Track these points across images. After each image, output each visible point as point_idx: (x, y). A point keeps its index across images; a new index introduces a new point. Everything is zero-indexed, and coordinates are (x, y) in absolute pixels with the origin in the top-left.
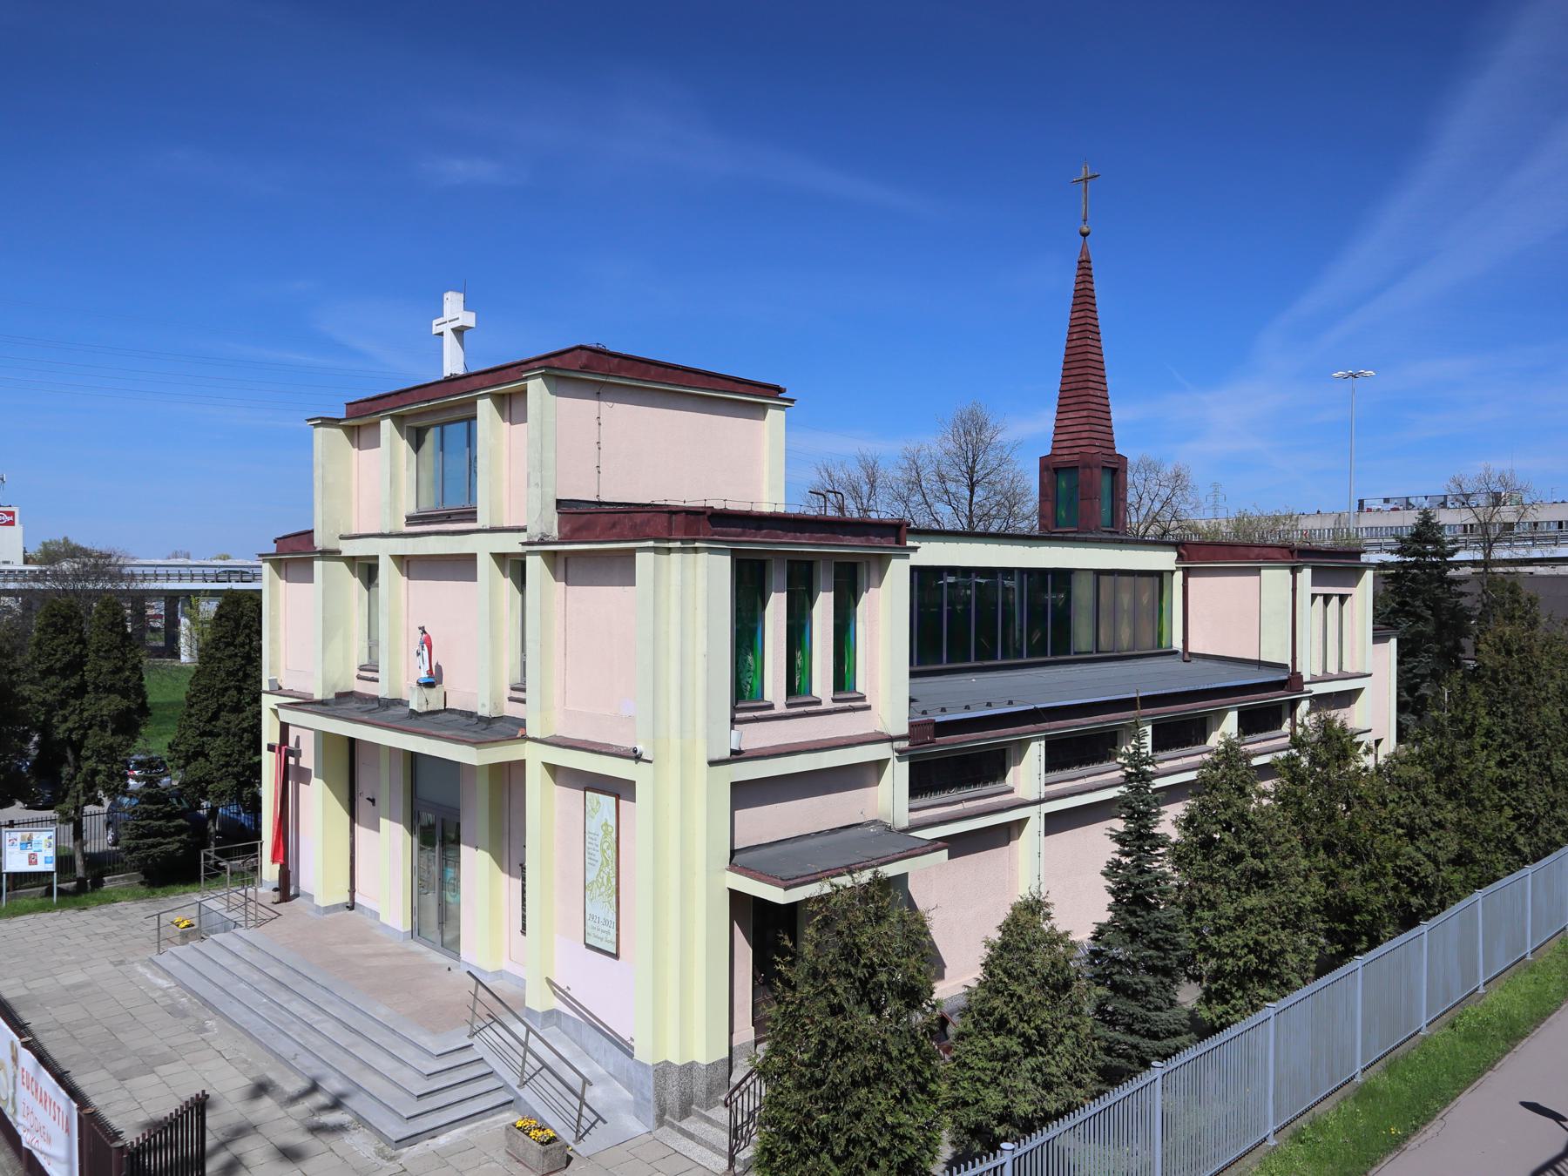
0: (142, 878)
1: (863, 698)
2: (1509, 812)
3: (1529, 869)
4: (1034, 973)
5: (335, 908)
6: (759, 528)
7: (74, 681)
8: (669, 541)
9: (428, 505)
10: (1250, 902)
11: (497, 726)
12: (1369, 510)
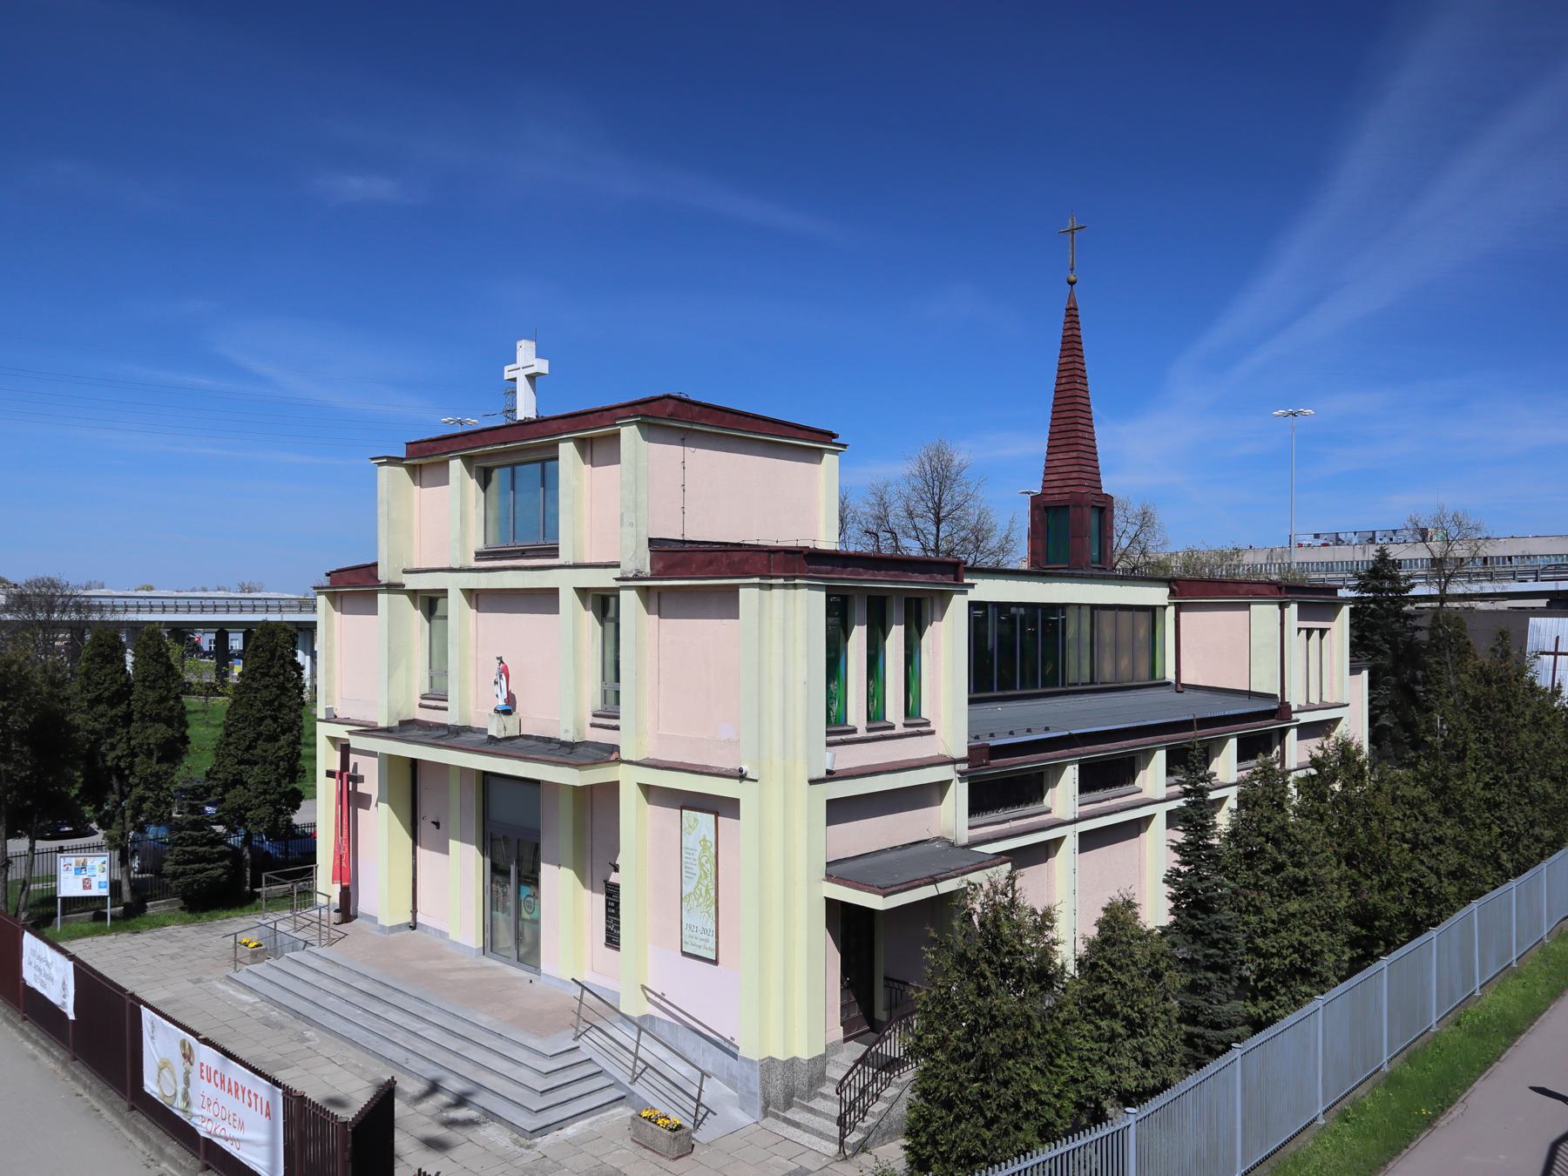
0: (182, 903)
1: (927, 724)
2: (1496, 830)
3: (1513, 883)
4: (1135, 963)
5: (399, 927)
6: (845, 566)
8: (772, 577)
9: (494, 543)
10: (1293, 906)
11: (581, 750)
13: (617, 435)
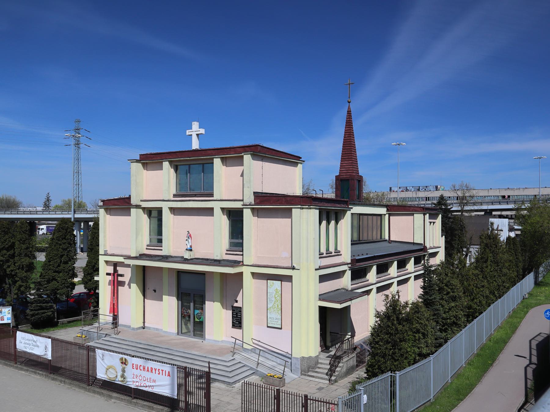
0: (31, 326)
5: (139, 328)
7: (12, 252)
12: (394, 191)
13: (242, 157)
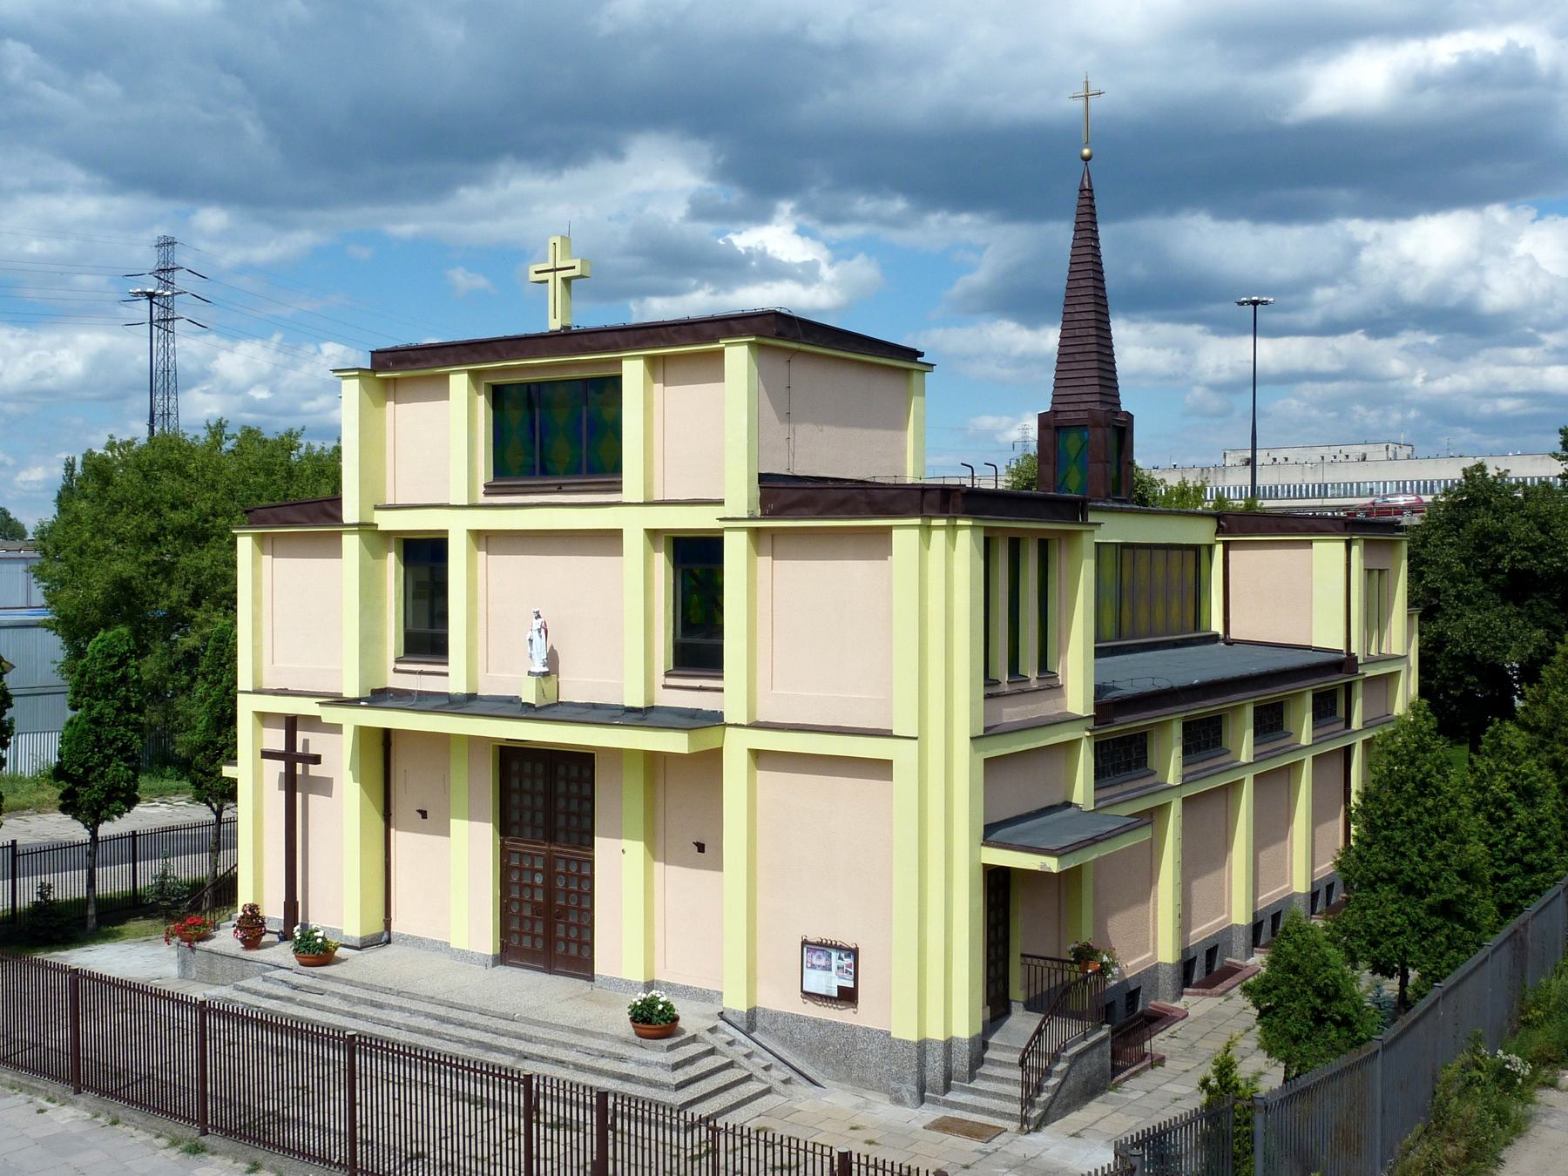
11: (653, 715)
13: (720, 354)
